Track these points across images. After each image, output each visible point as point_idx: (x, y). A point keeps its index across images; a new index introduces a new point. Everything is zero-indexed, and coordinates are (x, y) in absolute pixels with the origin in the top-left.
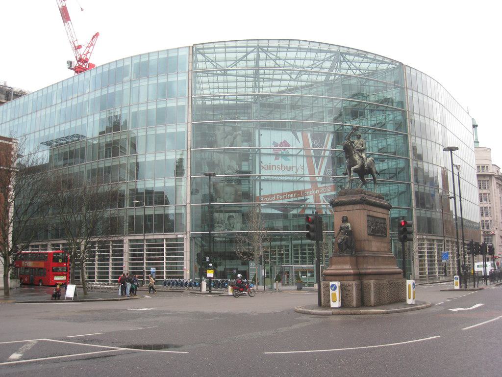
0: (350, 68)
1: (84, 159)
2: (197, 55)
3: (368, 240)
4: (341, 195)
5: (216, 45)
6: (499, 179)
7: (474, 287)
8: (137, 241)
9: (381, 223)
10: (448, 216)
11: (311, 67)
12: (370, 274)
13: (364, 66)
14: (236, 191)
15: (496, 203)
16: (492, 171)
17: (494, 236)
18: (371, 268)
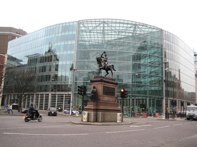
3: (102, 96)
5: (88, 21)
13: (146, 30)
18: (102, 107)
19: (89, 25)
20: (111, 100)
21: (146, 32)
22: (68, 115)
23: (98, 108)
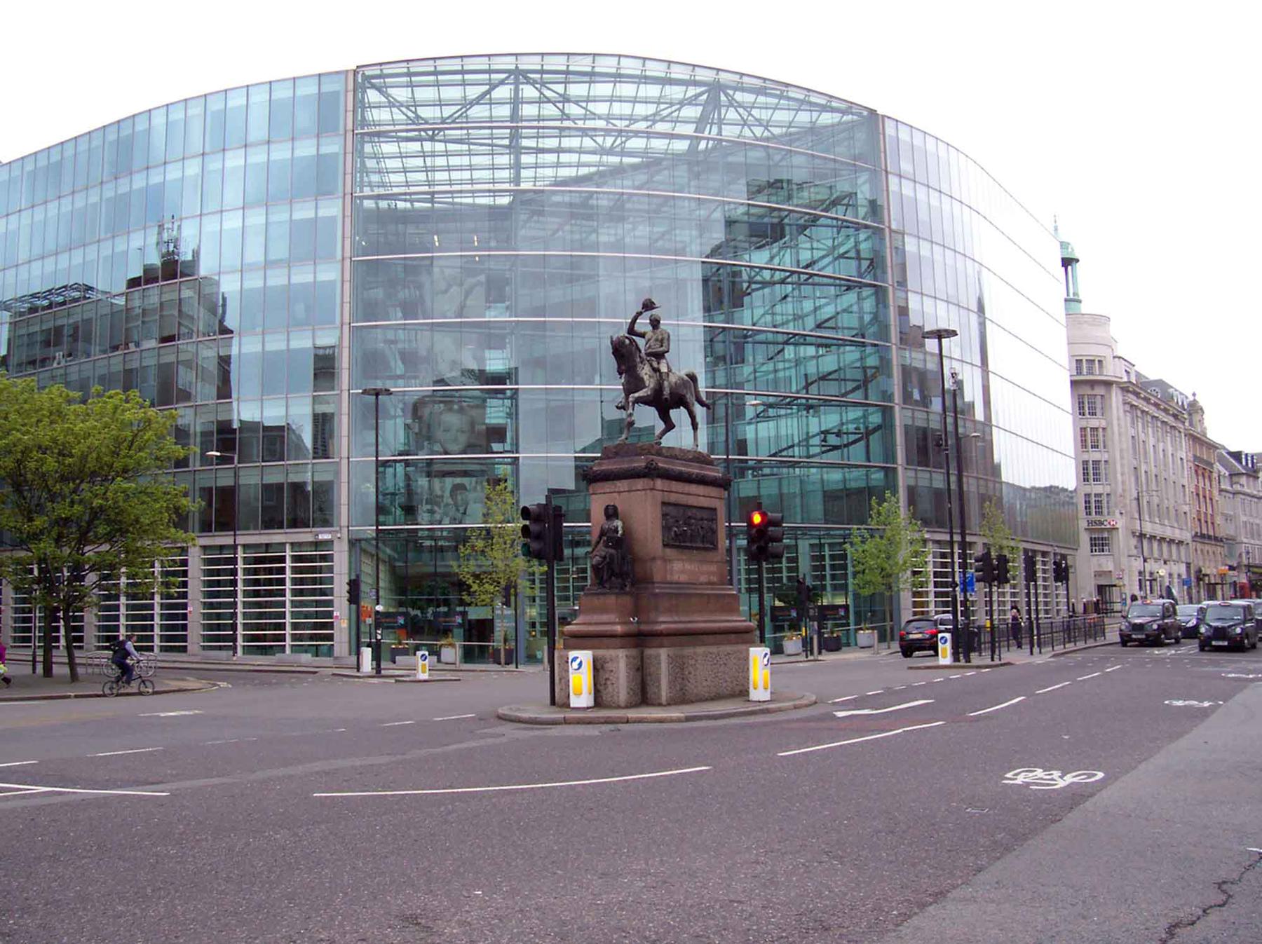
0: (745, 123)
1: (91, 344)
2: (368, 90)
4: (609, 458)
6: (1128, 391)
7: (993, 660)
8: (221, 548)
9: (702, 519)
10: (991, 485)
11: (653, 119)
12: (660, 634)
14: (472, 424)
15: (1121, 450)
16: (1113, 371)
17: (1114, 532)
18: (665, 622)
19: (424, 94)
20: (703, 579)
21: (776, 131)
22: (354, 673)
23: (644, 627)
